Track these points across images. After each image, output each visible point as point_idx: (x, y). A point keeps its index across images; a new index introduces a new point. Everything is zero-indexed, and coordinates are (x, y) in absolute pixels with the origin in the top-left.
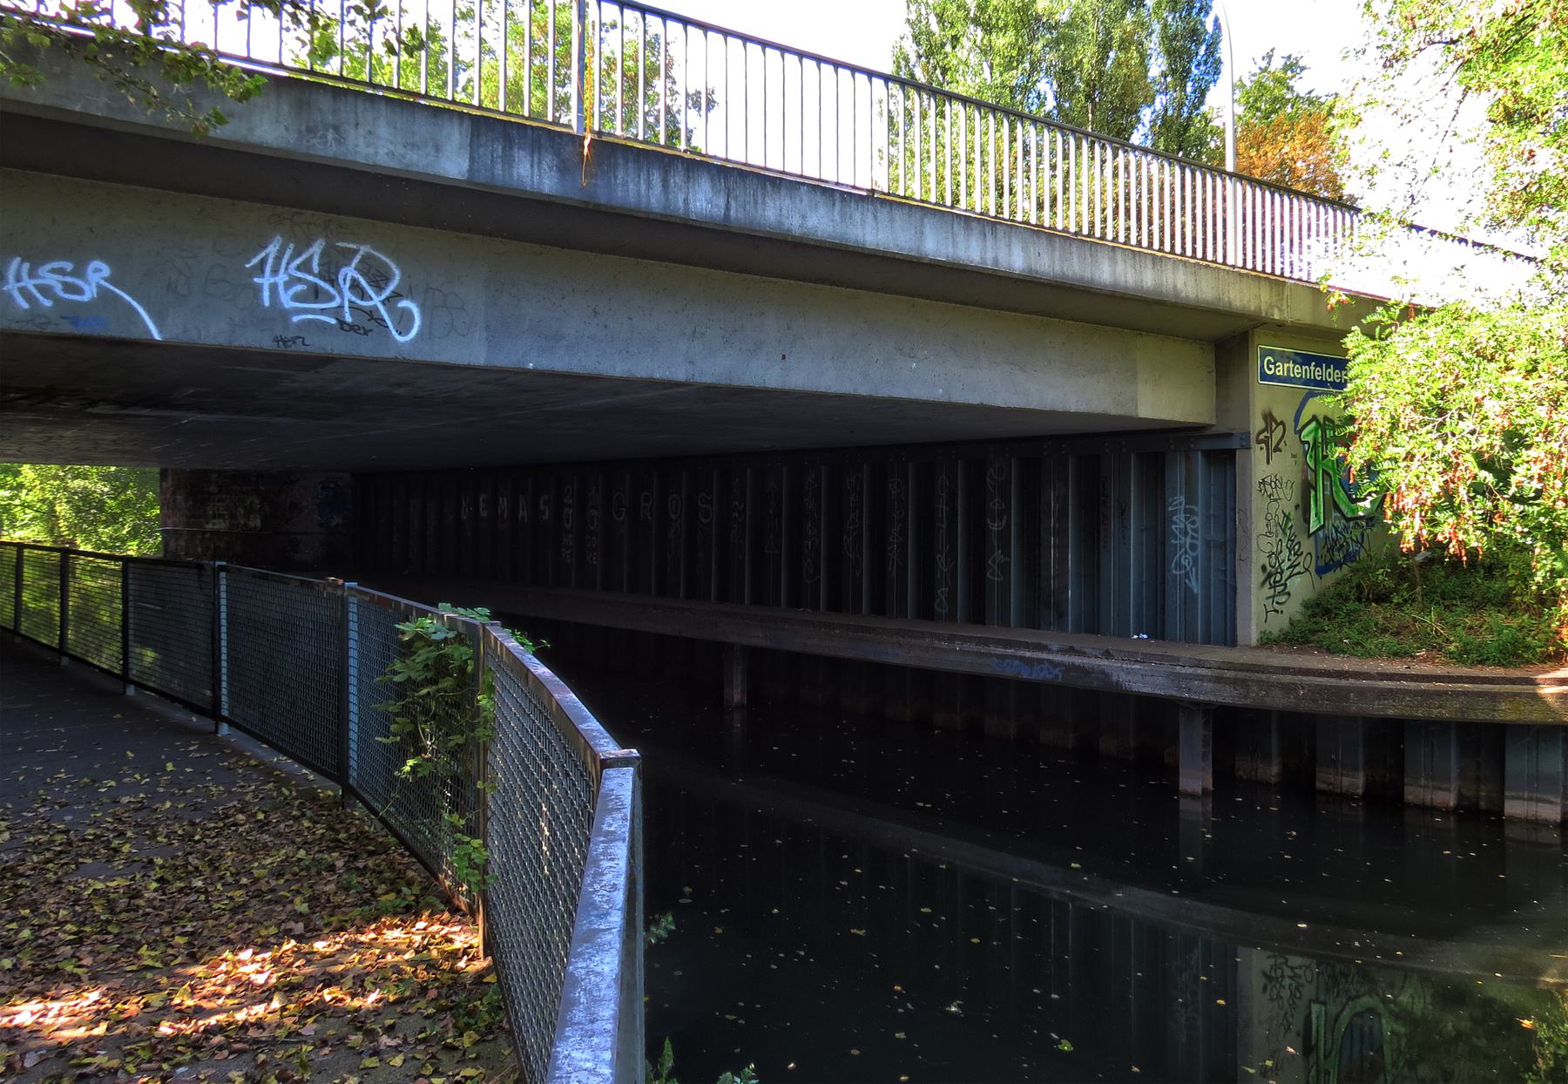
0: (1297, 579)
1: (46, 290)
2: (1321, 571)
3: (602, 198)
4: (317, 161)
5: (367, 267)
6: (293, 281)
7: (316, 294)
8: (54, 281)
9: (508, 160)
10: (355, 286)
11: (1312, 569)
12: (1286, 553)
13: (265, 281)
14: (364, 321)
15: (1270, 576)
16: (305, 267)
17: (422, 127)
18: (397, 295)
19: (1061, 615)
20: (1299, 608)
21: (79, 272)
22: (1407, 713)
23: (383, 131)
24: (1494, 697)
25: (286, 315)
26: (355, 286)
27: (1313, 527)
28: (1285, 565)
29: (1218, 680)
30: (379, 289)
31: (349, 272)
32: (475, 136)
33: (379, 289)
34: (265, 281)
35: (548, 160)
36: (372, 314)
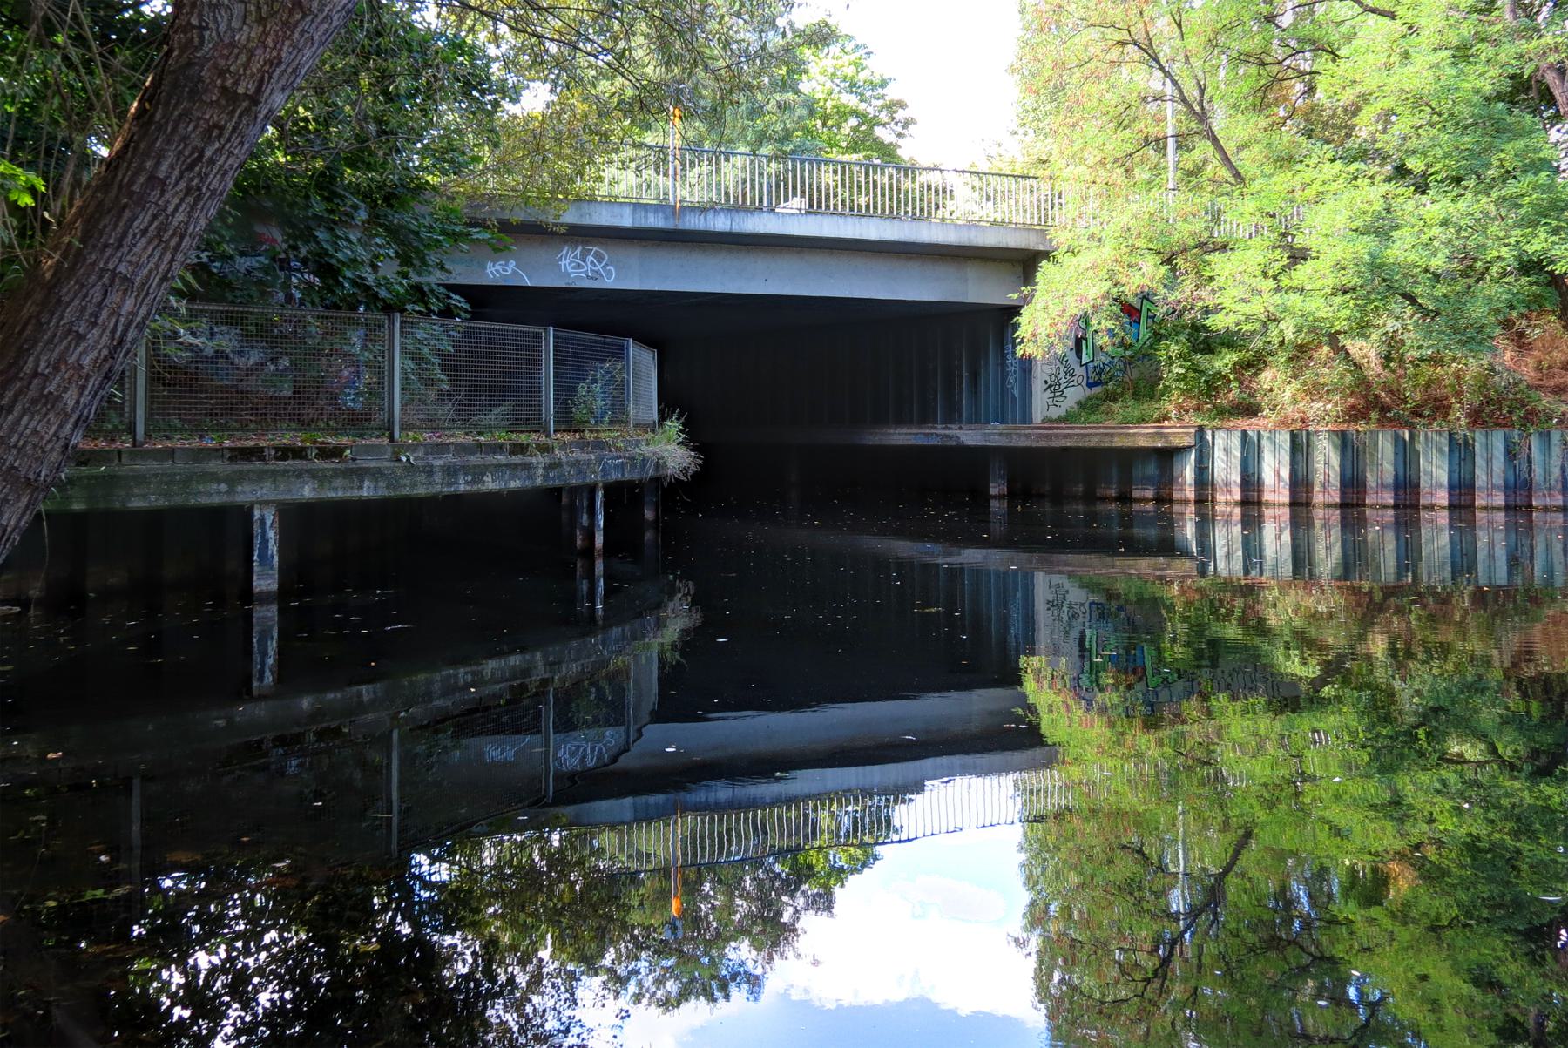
0: (1072, 389)
1: (497, 271)
2: (1090, 385)
3: (681, 227)
4: (996, 758)
5: (597, 255)
6: (571, 262)
7: (579, 266)
8: (499, 268)
9: (646, 217)
10: (592, 262)
11: (1084, 384)
12: (1062, 375)
13: (562, 263)
14: (596, 276)
15: (1050, 386)
16: (575, 257)
17: (617, 209)
18: (606, 265)
19: (961, 416)
20: (1073, 404)
21: (506, 265)
22: (1075, 444)
23: (604, 212)
24: (1112, 435)
25: (569, 274)
26: (592, 262)
27: (1085, 360)
28: (1062, 381)
29: (1000, 435)
30: (600, 262)
31: (590, 257)
32: (634, 210)
33: (600, 262)
34: (562, 263)
35: (661, 215)
36: (598, 273)
